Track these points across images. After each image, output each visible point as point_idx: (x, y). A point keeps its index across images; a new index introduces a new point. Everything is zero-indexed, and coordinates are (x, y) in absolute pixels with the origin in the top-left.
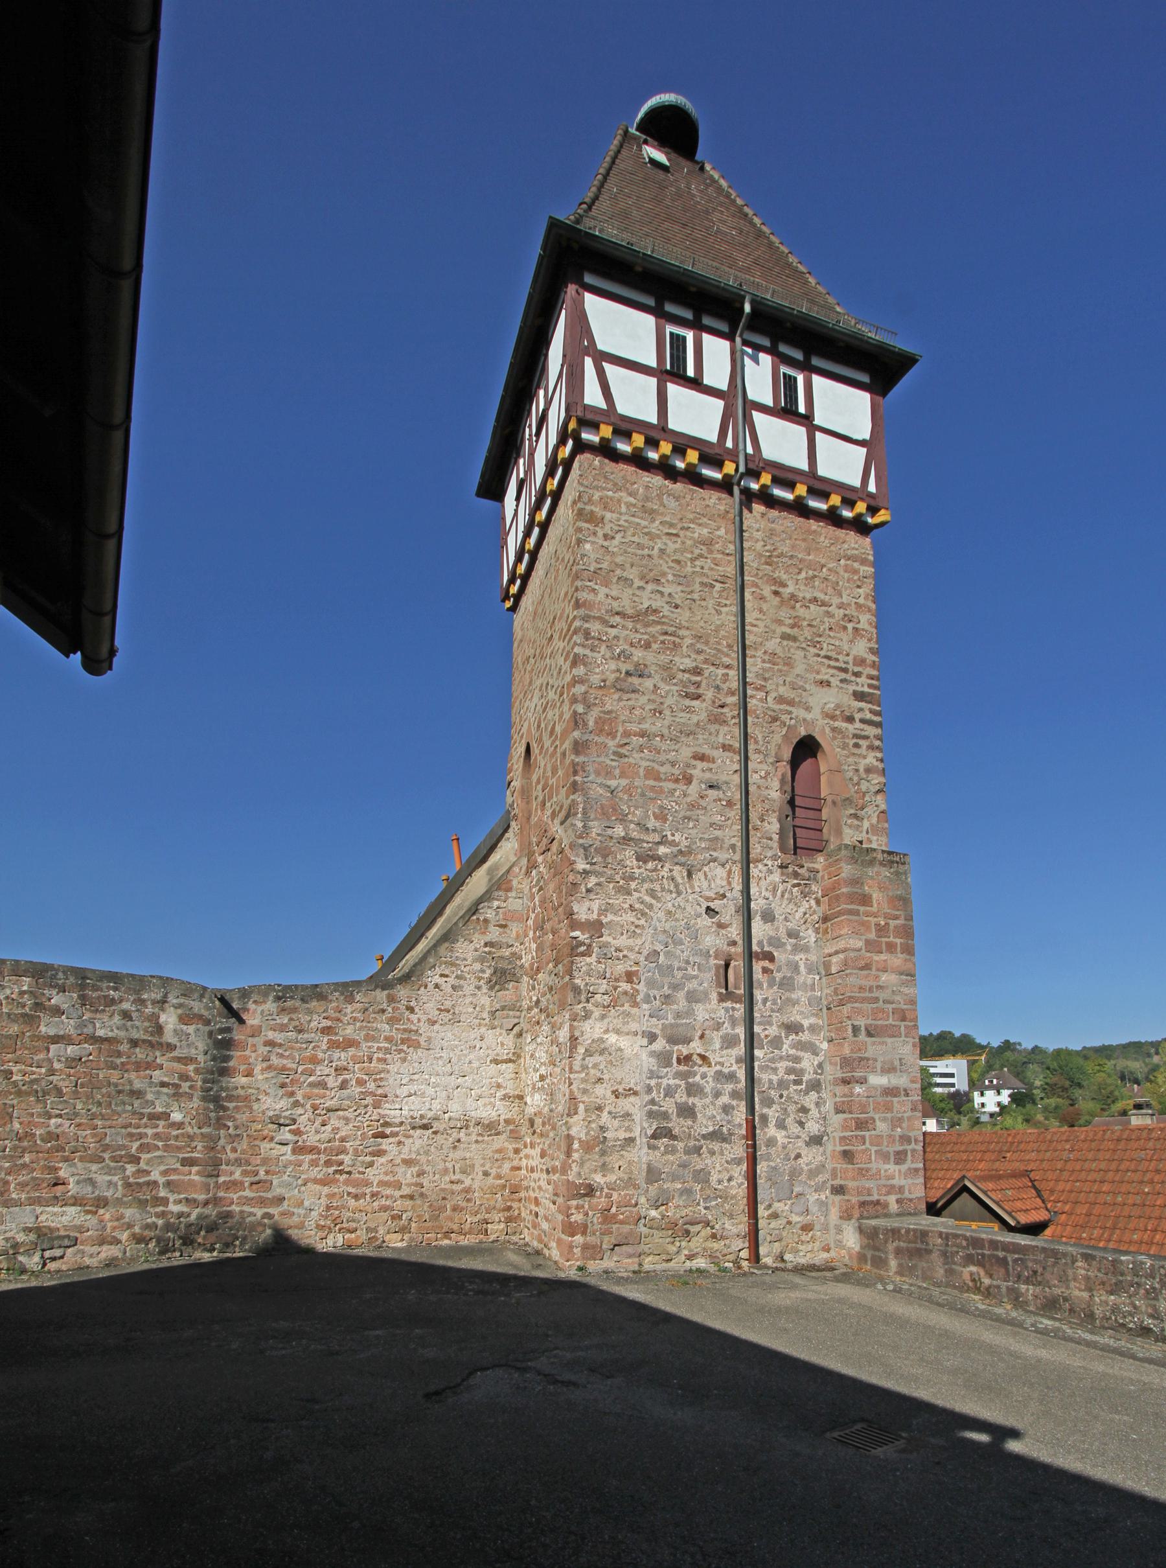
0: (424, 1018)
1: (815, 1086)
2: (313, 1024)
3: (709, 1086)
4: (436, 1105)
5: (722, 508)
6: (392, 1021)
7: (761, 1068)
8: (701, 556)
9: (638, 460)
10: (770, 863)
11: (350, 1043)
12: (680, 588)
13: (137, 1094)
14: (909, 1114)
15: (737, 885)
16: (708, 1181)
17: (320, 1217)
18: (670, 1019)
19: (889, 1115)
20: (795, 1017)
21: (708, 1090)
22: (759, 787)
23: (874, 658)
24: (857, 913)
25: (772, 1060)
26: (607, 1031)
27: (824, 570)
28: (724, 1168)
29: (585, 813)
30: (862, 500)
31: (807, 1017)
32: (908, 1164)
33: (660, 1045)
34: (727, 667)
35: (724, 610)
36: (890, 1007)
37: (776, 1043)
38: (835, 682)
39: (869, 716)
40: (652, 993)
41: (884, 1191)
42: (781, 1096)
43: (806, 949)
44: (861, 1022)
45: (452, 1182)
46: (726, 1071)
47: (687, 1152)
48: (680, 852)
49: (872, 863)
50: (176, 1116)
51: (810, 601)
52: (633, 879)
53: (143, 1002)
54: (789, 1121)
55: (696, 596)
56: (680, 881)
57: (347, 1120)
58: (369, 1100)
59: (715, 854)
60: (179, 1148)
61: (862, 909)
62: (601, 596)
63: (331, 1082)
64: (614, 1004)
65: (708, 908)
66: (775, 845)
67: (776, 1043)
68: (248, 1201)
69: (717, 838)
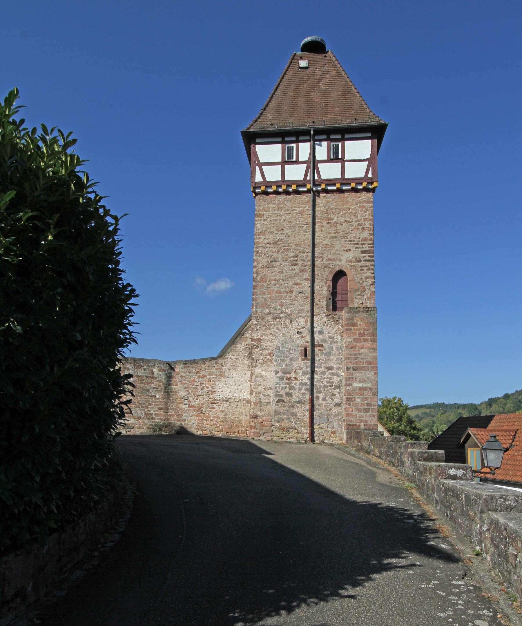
0: (226, 368)
1: (338, 387)
2: (194, 371)
4: (230, 394)
5: (307, 199)
6: (217, 369)
7: (317, 381)
8: (299, 218)
9: (276, 193)
10: (322, 315)
11: (204, 376)
13: (148, 390)
14: (372, 396)
15: (309, 323)
16: (296, 416)
17: (194, 424)
18: (284, 367)
19: (362, 397)
20: (331, 364)
21: (297, 388)
23: (371, 237)
24: (351, 330)
25: (321, 379)
26: (262, 371)
29: (256, 307)
30: (365, 181)
32: (370, 413)
33: (280, 374)
34: (308, 252)
35: (307, 234)
36: (364, 360)
37: (323, 373)
39: (368, 258)
40: (277, 359)
41: (358, 421)
42: (325, 390)
44: (351, 366)
46: (304, 382)
47: (289, 406)
48: (288, 315)
49: (358, 312)
50: (157, 396)
51: (343, 222)
52: (271, 325)
53: (149, 366)
54: (327, 398)
55: (296, 232)
57: (203, 398)
59: (300, 314)
60: (158, 405)
61: (352, 328)
62: (262, 240)
63: (199, 387)
65: (298, 332)
66: (324, 309)
67: (323, 373)
68: (176, 420)
69: (301, 309)
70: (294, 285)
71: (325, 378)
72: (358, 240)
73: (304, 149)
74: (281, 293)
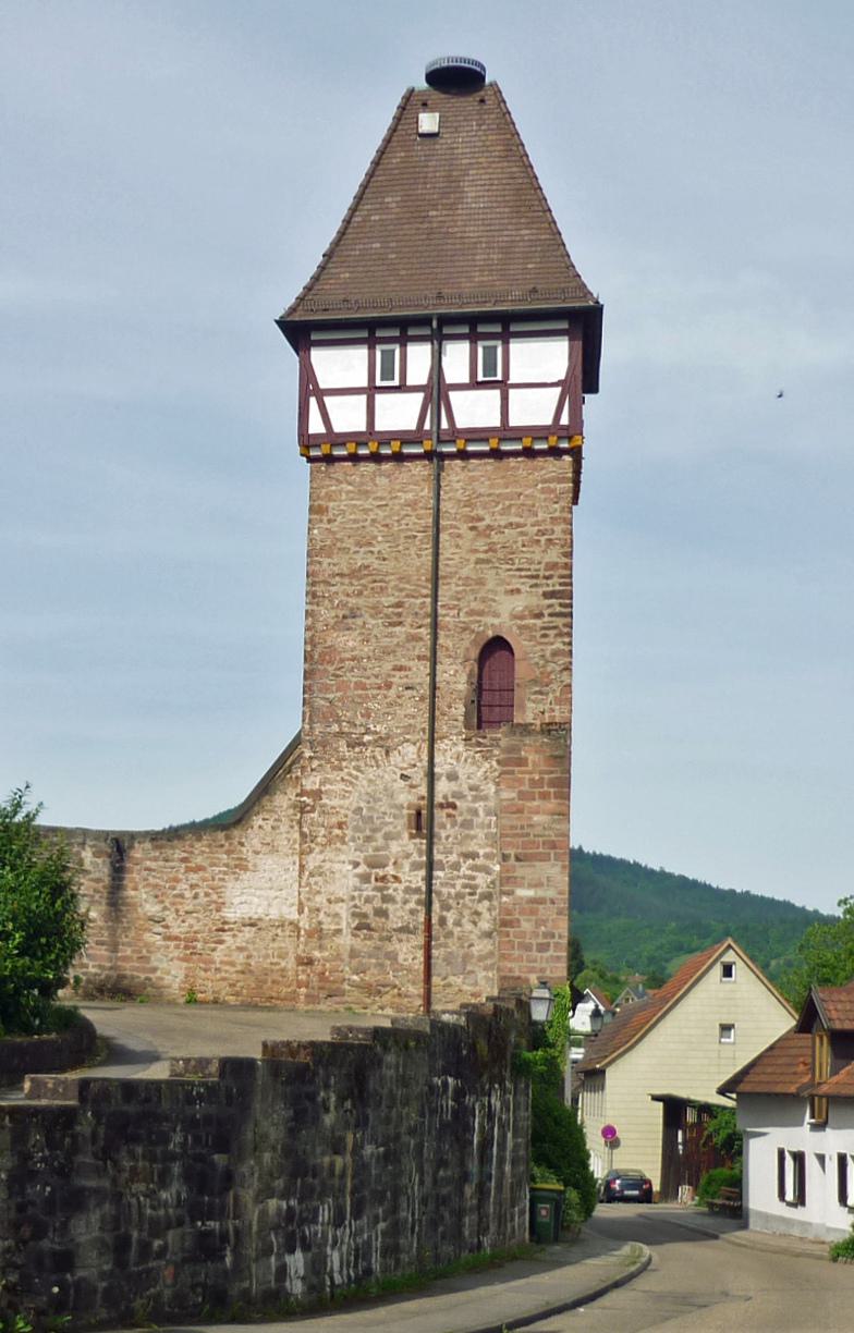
2: (176, 856)
3: (399, 896)
4: (260, 910)
5: (426, 473)
6: (228, 853)
8: (407, 515)
11: (199, 868)
12: (388, 545)
14: (555, 916)
15: (425, 757)
16: (396, 959)
18: (371, 852)
19: (534, 918)
20: (472, 847)
21: (398, 899)
22: (448, 683)
24: (512, 772)
25: (452, 878)
27: (522, 497)
28: (409, 952)
30: (553, 434)
31: (484, 848)
32: (551, 953)
33: (362, 869)
35: (423, 553)
36: (541, 839)
37: (456, 866)
38: (524, 588)
39: (558, 609)
40: (357, 835)
42: (458, 904)
43: (485, 798)
44: (512, 852)
45: (272, 964)
47: (381, 939)
51: (505, 527)
54: (464, 921)
56: (380, 758)
58: (213, 906)
59: (407, 737)
61: (516, 769)
62: (325, 565)
63: (188, 894)
64: (330, 842)
65: (402, 775)
66: (460, 724)
67: (456, 866)
68: (137, 969)
69: (410, 725)
70: (394, 670)
71: (459, 877)
72: (537, 567)
73: (418, 359)
74: (364, 689)
